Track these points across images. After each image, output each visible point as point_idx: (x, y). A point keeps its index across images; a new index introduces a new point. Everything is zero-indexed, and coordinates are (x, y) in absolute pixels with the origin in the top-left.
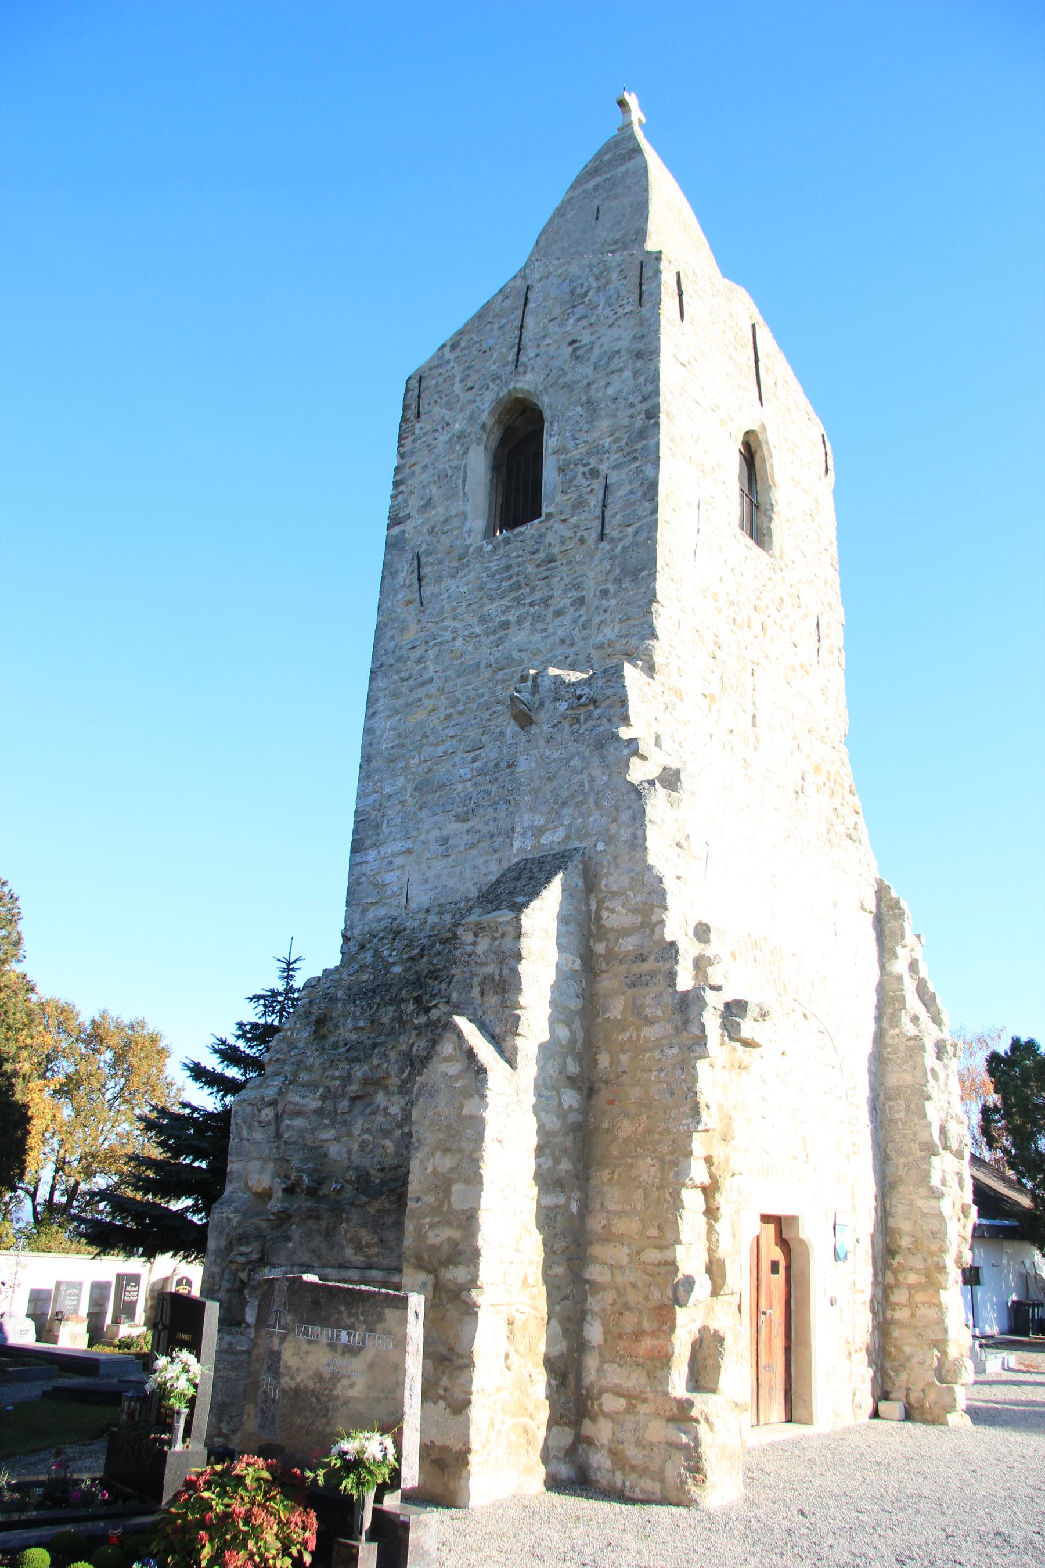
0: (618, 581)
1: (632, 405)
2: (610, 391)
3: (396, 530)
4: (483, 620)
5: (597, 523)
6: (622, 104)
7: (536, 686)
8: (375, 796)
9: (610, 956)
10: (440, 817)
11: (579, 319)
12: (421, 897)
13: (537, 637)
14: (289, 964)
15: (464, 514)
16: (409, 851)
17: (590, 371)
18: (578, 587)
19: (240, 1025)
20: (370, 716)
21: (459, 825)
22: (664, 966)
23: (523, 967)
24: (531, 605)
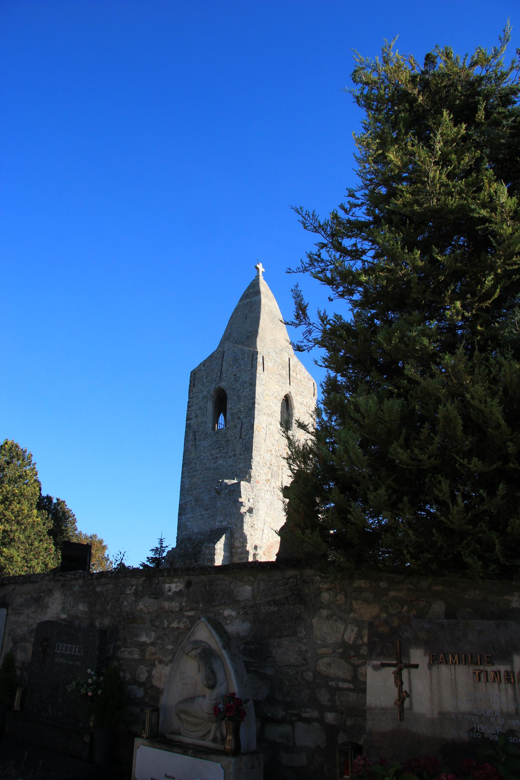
0: (244, 451)
1: (249, 400)
2: (244, 394)
3: (188, 422)
4: (211, 455)
5: (239, 433)
6: (257, 269)
7: (221, 485)
8: (184, 501)
9: (236, 552)
10: (201, 509)
11: (237, 368)
12: (196, 530)
13: (224, 463)
14: (161, 540)
15: (206, 422)
16: (193, 517)
17: (239, 386)
18: (234, 451)
19: (148, 558)
20: (182, 478)
21: (205, 512)
22: (246, 556)
23: (215, 557)
24: (223, 453)
